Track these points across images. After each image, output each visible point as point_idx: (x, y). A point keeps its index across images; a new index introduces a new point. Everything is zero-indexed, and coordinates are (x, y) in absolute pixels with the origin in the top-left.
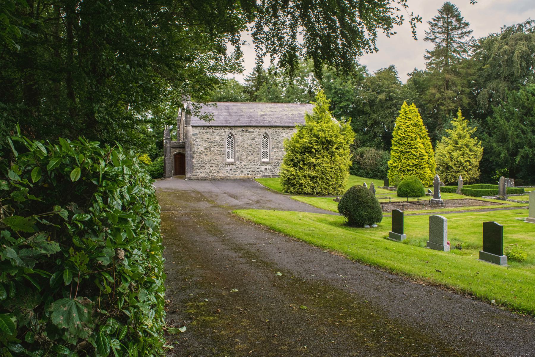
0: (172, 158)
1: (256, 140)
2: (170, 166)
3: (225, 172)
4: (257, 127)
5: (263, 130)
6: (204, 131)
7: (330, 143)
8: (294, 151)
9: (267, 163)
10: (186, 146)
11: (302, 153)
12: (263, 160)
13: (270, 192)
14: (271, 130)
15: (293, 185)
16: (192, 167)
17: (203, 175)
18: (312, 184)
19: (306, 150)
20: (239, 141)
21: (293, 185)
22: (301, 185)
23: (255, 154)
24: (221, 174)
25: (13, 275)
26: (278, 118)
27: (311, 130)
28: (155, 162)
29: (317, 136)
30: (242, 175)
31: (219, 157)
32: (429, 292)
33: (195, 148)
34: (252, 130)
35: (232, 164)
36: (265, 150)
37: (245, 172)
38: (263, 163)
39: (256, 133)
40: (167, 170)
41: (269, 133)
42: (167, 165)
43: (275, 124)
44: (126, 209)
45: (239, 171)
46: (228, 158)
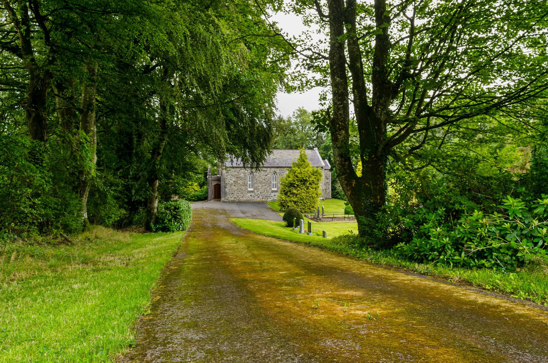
1: (269, 176)
2: (211, 194)
3: (248, 197)
4: (269, 167)
5: (273, 170)
6: (234, 170)
7: (306, 181)
8: (285, 185)
9: (276, 191)
10: (222, 180)
12: (273, 189)
13: (270, 210)
14: (278, 169)
15: (284, 206)
16: (226, 194)
17: (233, 199)
19: (291, 185)
20: (257, 177)
21: (284, 206)
22: (288, 206)
23: (267, 185)
24: (244, 199)
25: (389, 10)
28: (202, 189)
29: (297, 176)
30: (259, 199)
31: (243, 187)
33: (227, 182)
34: (266, 169)
35: (252, 192)
36: (274, 183)
37: (261, 197)
38: (273, 191)
39: (268, 171)
40: (209, 195)
41: (277, 172)
42: (209, 192)
44: (107, 115)
45: (256, 197)
46: (250, 188)
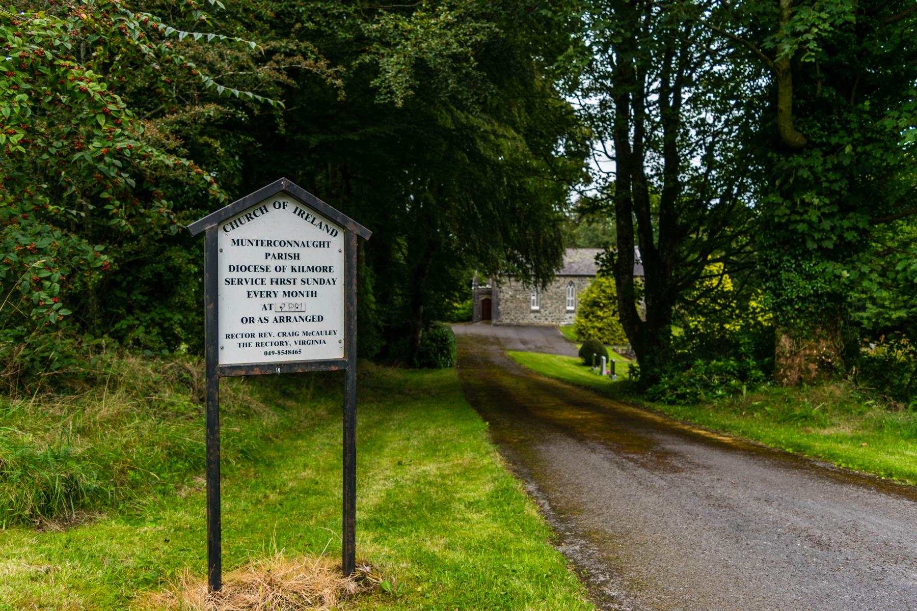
0: (480, 304)
2: (477, 313)
5: (569, 279)
11: (592, 307)
15: (583, 335)
16: (498, 313)
17: (508, 321)
18: (600, 335)
19: (595, 304)
21: (583, 335)
22: (590, 335)
24: (526, 321)
26: (585, 266)
27: (601, 286)
31: (524, 305)
32: (16, 448)
33: (501, 296)
37: (550, 319)
38: (568, 312)
43: (582, 273)
45: (543, 319)
